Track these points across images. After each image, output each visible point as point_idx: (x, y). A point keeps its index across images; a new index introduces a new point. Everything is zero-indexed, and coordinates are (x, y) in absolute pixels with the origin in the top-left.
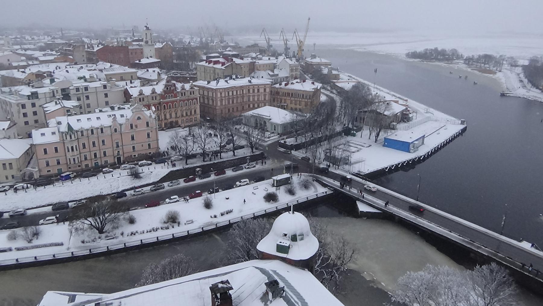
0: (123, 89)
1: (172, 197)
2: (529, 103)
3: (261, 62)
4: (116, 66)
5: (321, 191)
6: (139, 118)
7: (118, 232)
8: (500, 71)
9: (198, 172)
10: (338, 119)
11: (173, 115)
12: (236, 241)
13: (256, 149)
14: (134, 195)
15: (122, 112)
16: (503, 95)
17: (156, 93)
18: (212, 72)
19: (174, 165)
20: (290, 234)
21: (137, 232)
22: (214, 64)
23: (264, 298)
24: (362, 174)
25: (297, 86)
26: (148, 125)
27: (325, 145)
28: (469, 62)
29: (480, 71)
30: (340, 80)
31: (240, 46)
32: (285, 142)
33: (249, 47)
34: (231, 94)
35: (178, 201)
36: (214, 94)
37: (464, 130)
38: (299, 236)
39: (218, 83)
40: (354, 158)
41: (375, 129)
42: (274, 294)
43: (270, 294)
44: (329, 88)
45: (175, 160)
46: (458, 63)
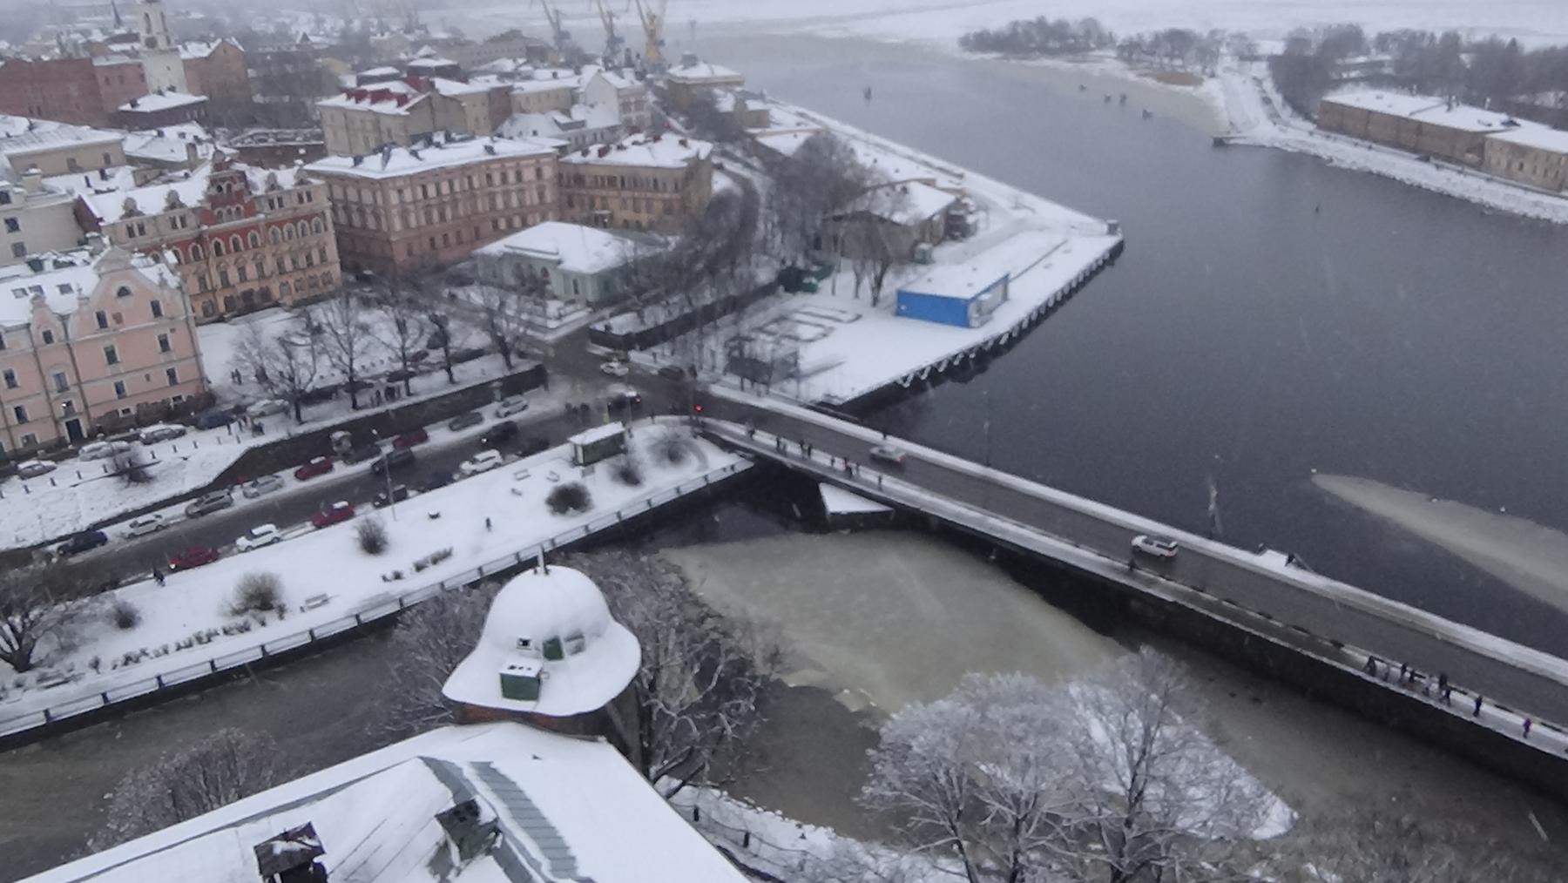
0: (70, 200)
1: (255, 532)
2: (1291, 163)
3: (529, 87)
4: (48, 126)
5: (718, 464)
6: (123, 292)
7: (80, 659)
8: (1213, 75)
9: (339, 443)
10: (764, 248)
11: (251, 271)
12: (378, 677)
13: (522, 355)
14: (132, 536)
15: (65, 276)
16: (1219, 143)
17: (182, 205)
18: (369, 126)
19: (258, 430)
20: (537, 640)
21: (144, 653)
22: (373, 102)
23: (439, 863)
24: (836, 402)
25: (636, 155)
26: (157, 311)
27: (726, 328)
28: (1131, 54)
29: (1159, 79)
30: (774, 128)
31: (468, 38)
32: (608, 327)
33: (493, 40)
34: (432, 191)
35: (278, 540)
36: (379, 195)
37: (1116, 252)
38: (569, 640)
39: (386, 159)
40: (810, 357)
41: (869, 264)
42: (466, 847)
43: (454, 850)
44: (739, 154)
45: (262, 415)
46: (1100, 59)
